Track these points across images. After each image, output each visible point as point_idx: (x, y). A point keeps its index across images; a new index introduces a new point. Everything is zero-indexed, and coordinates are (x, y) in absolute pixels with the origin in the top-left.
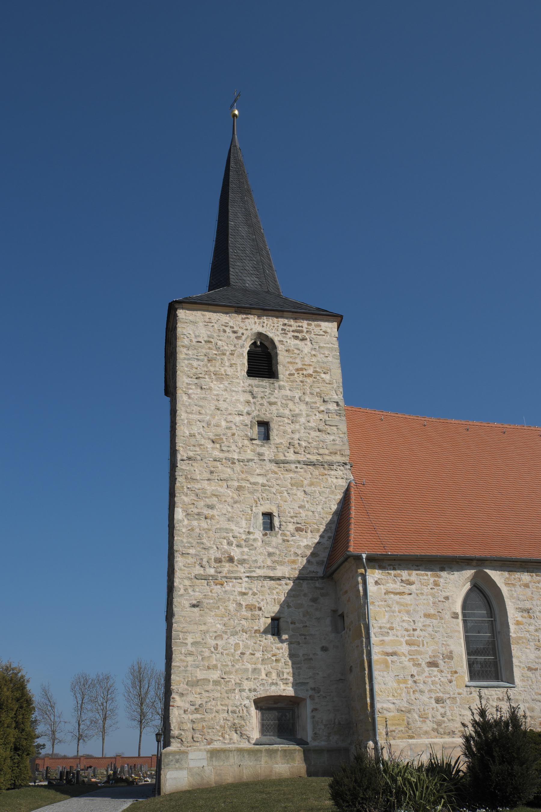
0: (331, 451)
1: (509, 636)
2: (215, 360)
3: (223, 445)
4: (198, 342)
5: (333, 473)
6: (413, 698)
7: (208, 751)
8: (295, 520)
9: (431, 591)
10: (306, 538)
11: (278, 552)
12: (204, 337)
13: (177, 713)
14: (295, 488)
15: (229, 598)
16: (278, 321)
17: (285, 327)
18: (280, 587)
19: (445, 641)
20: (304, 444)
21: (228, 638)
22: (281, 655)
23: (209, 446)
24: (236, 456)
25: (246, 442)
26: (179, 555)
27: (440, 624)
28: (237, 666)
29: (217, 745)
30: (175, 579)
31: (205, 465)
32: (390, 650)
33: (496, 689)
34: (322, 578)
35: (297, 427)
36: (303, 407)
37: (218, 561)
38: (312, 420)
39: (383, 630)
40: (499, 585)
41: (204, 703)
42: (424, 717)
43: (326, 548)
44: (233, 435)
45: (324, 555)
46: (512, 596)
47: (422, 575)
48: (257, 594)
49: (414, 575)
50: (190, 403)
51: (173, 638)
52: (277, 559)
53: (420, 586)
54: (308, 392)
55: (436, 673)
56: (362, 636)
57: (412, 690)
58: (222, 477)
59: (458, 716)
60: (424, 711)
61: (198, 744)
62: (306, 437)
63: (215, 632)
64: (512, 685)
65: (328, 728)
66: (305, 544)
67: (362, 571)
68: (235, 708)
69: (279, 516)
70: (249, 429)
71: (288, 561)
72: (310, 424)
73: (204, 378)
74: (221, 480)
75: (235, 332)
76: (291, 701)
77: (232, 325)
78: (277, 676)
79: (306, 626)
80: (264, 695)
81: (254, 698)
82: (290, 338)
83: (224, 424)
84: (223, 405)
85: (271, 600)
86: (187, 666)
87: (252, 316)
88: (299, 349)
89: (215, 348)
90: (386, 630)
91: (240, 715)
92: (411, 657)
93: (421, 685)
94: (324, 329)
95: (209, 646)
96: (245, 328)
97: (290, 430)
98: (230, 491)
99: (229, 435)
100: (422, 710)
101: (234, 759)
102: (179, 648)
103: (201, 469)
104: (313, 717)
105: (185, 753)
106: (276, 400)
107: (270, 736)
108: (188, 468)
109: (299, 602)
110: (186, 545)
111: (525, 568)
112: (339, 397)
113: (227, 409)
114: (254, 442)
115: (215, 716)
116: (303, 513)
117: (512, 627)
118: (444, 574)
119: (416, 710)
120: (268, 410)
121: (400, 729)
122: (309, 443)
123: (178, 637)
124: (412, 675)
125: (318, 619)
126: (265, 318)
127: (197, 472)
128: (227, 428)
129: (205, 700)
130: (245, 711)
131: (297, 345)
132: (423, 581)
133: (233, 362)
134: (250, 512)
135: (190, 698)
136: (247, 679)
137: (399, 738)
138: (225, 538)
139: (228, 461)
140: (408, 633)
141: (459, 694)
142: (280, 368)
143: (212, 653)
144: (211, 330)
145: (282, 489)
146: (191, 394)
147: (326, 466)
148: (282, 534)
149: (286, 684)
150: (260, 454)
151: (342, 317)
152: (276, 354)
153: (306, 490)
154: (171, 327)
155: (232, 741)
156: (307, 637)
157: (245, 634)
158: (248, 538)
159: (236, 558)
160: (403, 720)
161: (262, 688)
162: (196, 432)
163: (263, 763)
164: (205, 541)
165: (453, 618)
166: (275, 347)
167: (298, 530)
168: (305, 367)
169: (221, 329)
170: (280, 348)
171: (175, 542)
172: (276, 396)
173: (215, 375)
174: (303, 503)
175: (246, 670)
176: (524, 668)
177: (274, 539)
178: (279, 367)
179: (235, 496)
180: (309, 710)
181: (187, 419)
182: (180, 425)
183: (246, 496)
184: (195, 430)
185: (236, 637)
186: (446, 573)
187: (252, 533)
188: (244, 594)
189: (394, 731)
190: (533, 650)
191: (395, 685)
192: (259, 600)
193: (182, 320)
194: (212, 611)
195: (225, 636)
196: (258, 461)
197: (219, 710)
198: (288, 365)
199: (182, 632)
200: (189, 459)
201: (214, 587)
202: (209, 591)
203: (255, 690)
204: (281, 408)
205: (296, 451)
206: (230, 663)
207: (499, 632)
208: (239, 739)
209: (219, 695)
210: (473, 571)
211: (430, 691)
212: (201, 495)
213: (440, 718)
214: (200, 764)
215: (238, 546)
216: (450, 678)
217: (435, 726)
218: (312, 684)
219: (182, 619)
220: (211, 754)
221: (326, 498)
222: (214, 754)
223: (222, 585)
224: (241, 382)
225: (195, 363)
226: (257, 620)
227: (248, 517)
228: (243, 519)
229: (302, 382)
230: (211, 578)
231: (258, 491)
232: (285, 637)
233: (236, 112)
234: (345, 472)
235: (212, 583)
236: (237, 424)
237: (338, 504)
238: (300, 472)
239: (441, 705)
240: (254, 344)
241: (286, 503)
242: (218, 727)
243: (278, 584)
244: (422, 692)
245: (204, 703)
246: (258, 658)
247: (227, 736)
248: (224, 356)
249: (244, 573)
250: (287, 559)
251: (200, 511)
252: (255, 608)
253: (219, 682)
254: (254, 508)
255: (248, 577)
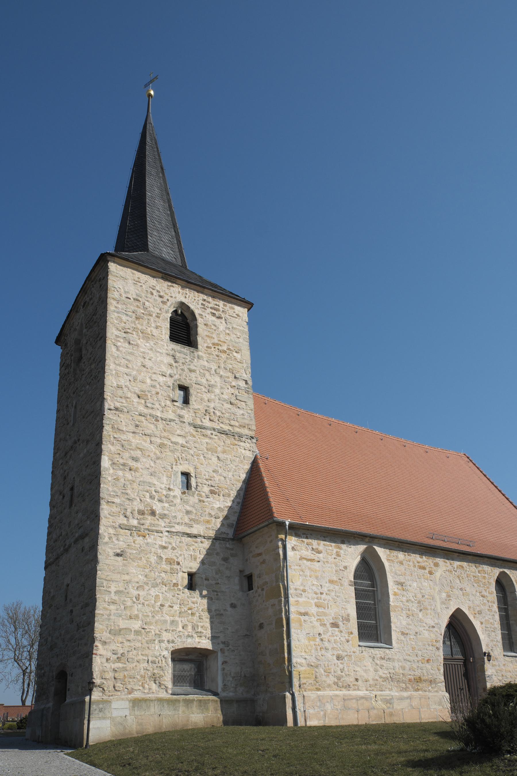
0: (241, 424)
1: (389, 604)
2: (142, 319)
3: (147, 401)
4: (127, 298)
5: (242, 444)
6: (320, 654)
7: (130, 701)
8: (210, 482)
9: (334, 560)
10: (219, 501)
11: (194, 511)
12: (132, 295)
13: (99, 662)
14: (210, 453)
15: (151, 550)
16: (199, 296)
17: (204, 303)
18: (196, 545)
19: (344, 605)
20: (218, 413)
21: (149, 589)
22: (196, 609)
23: (135, 400)
24: (159, 414)
25: (168, 403)
26: (105, 503)
27: (340, 590)
28: (157, 618)
29: (137, 695)
30: (100, 526)
31: (131, 418)
32: (303, 611)
33: (380, 649)
34: (233, 540)
35: (213, 397)
36: (218, 379)
37: (141, 513)
38: (225, 393)
39: (297, 592)
40: (383, 560)
41: (126, 652)
42: (328, 672)
43: (235, 512)
44: (157, 393)
45: (234, 519)
46: (391, 570)
47: (328, 546)
48: (176, 549)
49: (321, 545)
50: (118, 355)
51: (97, 585)
52: (194, 517)
53: (326, 554)
54: (222, 366)
55: (337, 633)
56: (280, 596)
57: (319, 648)
58: (146, 432)
59: (353, 672)
60: (328, 666)
61: (119, 693)
62: (220, 407)
63: (138, 582)
64: (390, 647)
65: (236, 680)
66: (218, 506)
67: (283, 536)
68: (155, 659)
69: (196, 477)
70: (171, 391)
71: (203, 521)
72: (223, 396)
73: (132, 334)
74: (145, 435)
75: (161, 297)
76: (200, 654)
77: (159, 290)
78: (193, 630)
79: (218, 583)
80: (181, 647)
81: (172, 649)
82: (208, 314)
83: (148, 381)
84: (149, 364)
85: (192, 556)
86: (110, 615)
87: (177, 286)
88: (215, 326)
89: (142, 307)
90: (300, 592)
91: (159, 665)
92: (319, 618)
93: (326, 643)
94: (237, 312)
95: (131, 596)
96: (170, 295)
97: (206, 399)
98: (154, 446)
99: (153, 393)
100: (326, 666)
101: (154, 709)
102: (103, 596)
103: (127, 421)
104: (223, 669)
105: (109, 702)
106: (195, 368)
107: (186, 686)
108: (115, 418)
109: (212, 560)
110: (112, 493)
111: (400, 548)
112: (247, 376)
113: (152, 368)
114: (175, 404)
115: (136, 666)
116: (217, 478)
117: (392, 597)
118: (344, 546)
119: (323, 665)
120: (188, 376)
121: (310, 682)
122: (223, 414)
123: (102, 585)
124: (319, 634)
125: (228, 578)
126: (187, 290)
127: (124, 423)
128: (151, 386)
129: (127, 649)
130: (164, 661)
131: (214, 321)
132: (328, 551)
133: (159, 324)
134: (170, 469)
135: (113, 647)
136: (166, 630)
137: (309, 690)
138: (147, 492)
139: (152, 418)
140: (317, 596)
141: (354, 652)
142: (199, 339)
143: (134, 603)
144: (140, 289)
145: (199, 452)
146: (120, 346)
147: (237, 437)
148: (198, 494)
149: (200, 637)
150: (180, 416)
151: (252, 304)
152: (196, 326)
153: (220, 456)
154: (93, 278)
155: (151, 691)
156: (219, 594)
157: (164, 586)
158: (169, 494)
159: (157, 512)
160: (312, 674)
161: (180, 640)
162: (123, 384)
163: (180, 713)
164: (129, 491)
165: (350, 585)
166: (195, 319)
167: (212, 492)
168: (220, 343)
169: (149, 291)
170: (200, 321)
171: (101, 489)
172: (195, 365)
173: (142, 333)
174: (216, 468)
175: (165, 621)
176: (399, 632)
177: (191, 498)
178: (198, 338)
179: (158, 452)
180: (220, 663)
181: (115, 370)
182: (108, 375)
183: (168, 454)
184: (122, 382)
185: (156, 589)
186: (345, 545)
187: (172, 490)
188: (165, 548)
189: (305, 684)
190: (405, 617)
191: (306, 642)
192: (177, 555)
193: (113, 274)
194: (134, 561)
195: (147, 588)
196: (179, 422)
197: (140, 659)
198: (207, 338)
199: (106, 580)
200: (117, 409)
201: (136, 538)
202: (132, 541)
203: (173, 642)
204: (199, 376)
205: (212, 418)
206: (150, 614)
207: (380, 601)
208: (157, 689)
209: (140, 645)
210: (365, 546)
211: (333, 648)
212: (127, 446)
213: (339, 673)
214: (123, 713)
215: (160, 501)
216: (347, 638)
217: (336, 681)
218: (222, 639)
219: (106, 567)
220: (133, 703)
221: (236, 466)
222: (136, 703)
223: (144, 537)
224: (166, 345)
225: (124, 318)
226: (176, 574)
227: (169, 474)
228: (165, 475)
229: (217, 356)
230: (134, 529)
231: (178, 450)
232: (205, 592)
233: (152, 92)
234: (252, 445)
235: (135, 534)
236: (161, 384)
237: (247, 473)
238: (215, 439)
239: (341, 661)
240: (175, 312)
241: (202, 466)
242: (138, 677)
243: (193, 541)
244: (327, 649)
245: (126, 652)
246: (176, 611)
247: (146, 686)
248: (150, 317)
249: (165, 527)
250: (202, 518)
251: (125, 462)
252: (174, 562)
253: (140, 632)
254: (174, 467)
255: (168, 532)
